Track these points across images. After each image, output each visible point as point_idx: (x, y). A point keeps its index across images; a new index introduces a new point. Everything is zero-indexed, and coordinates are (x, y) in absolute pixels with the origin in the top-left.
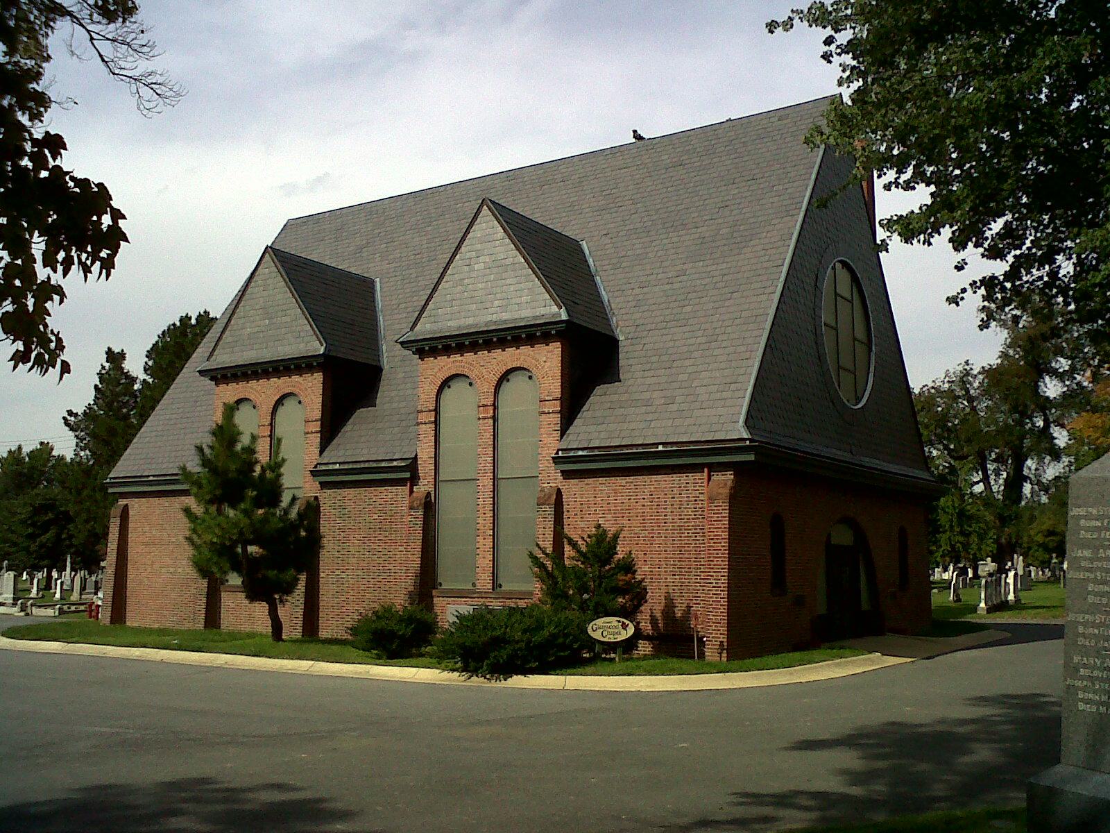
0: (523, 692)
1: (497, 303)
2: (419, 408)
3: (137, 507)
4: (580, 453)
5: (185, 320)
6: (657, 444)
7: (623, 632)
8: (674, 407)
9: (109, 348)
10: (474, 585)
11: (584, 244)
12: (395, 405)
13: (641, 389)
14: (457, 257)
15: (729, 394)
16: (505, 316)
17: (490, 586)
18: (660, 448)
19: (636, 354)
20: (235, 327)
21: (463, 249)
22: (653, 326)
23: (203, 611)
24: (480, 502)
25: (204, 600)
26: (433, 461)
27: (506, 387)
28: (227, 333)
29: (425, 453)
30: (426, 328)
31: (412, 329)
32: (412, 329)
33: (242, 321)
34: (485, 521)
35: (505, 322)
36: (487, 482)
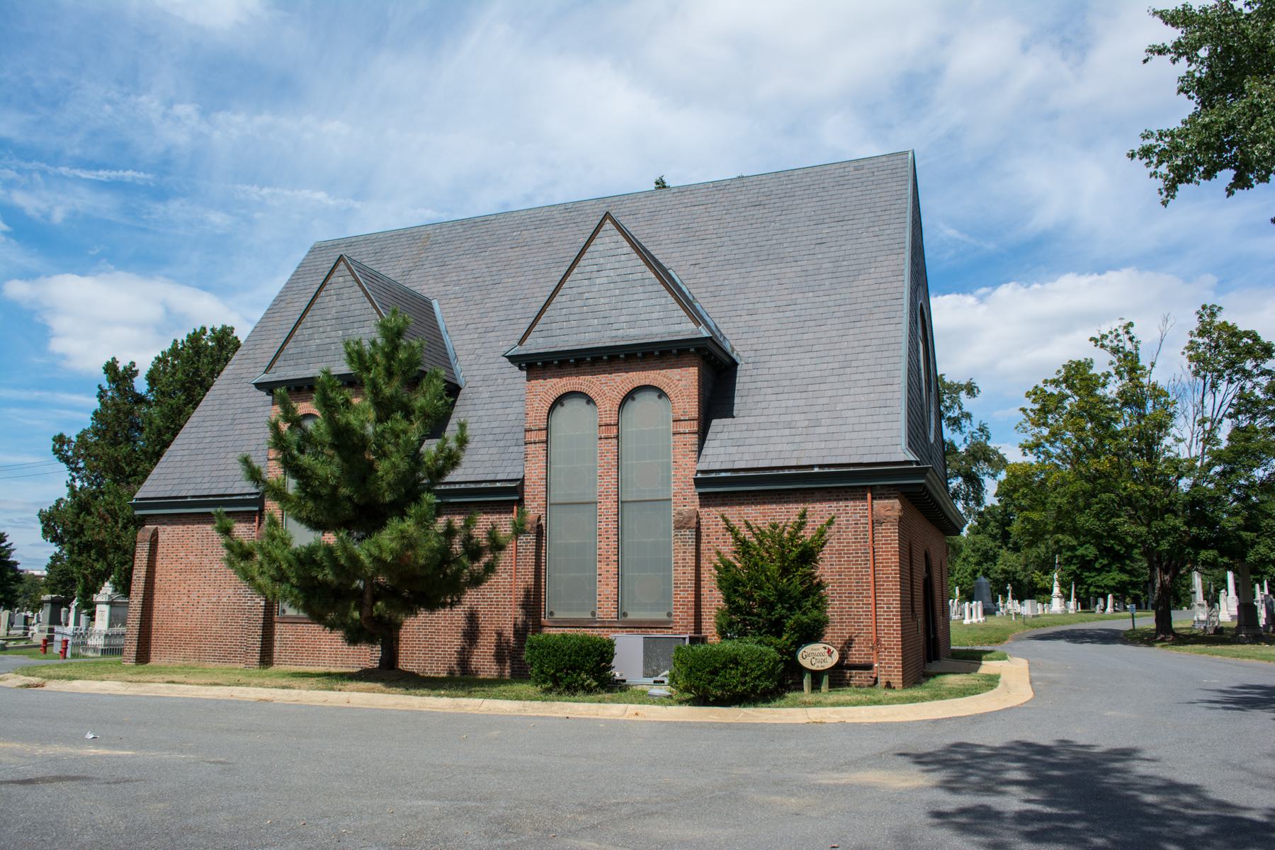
0: (613, 726)
1: (623, 319)
2: (527, 426)
3: (168, 533)
4: (723, 474)
5: (195, 338)
6: (812, 467)
7: (829, 659)
8: (823, 430)
9: (114, 359)
10: (593, 614)
11: (435, 304)
12: (485, 425)
13: (778, 411)
14: (575, 270)
15: (881, 418)
16: (632, 332)
17: (614, 614)
18: (816, 470)
19: (763, 378)
20: (300, 338)
21: (581, 263)
22: (775, 352)
23: (259, 644)
24: (603, 526)
25: (260, 632)
26: (543, 482)
27: (631, 406)
28: (291, 344)
29: (534, 474)
30: (537, 344)
31: (521, 342)
32: (521, 342)
33: (310, 331)
34: (606, 546)
35: (634, 337)
36: (608, 506)
